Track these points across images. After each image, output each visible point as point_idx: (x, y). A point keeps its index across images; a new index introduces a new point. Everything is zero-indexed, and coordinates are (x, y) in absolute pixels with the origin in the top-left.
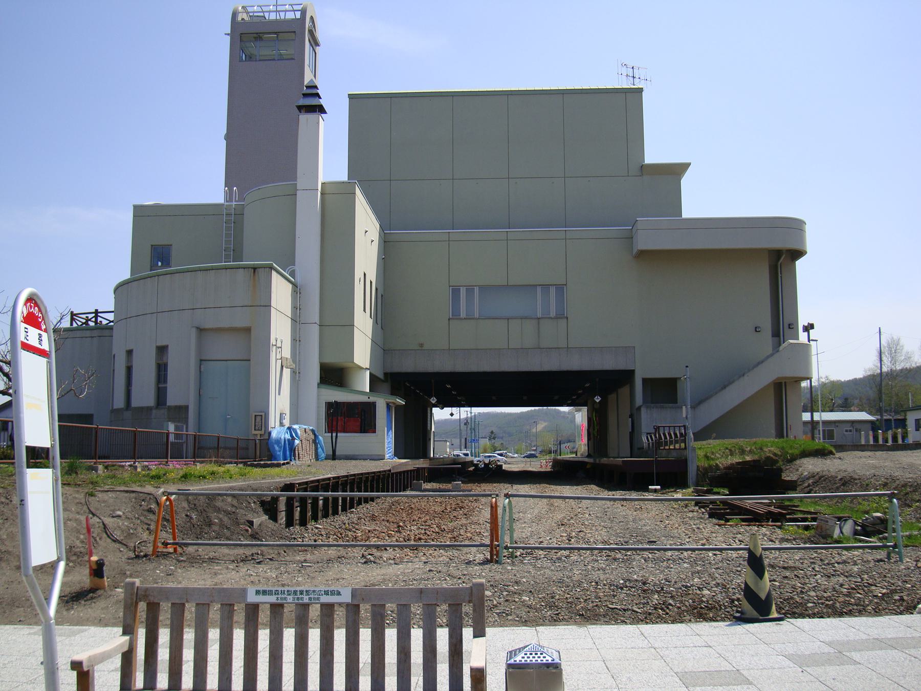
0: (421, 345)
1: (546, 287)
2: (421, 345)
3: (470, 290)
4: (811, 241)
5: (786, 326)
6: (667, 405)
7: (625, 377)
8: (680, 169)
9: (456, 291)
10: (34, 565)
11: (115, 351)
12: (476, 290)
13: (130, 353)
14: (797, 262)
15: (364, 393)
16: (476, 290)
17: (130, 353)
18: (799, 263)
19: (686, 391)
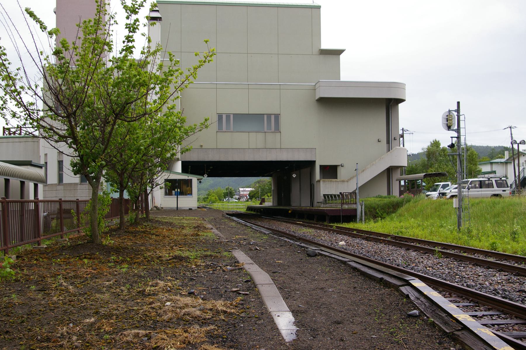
0: (201, 146)
1: (269, 116)
2: (201, 146)
3: (228, 116)
4: (408, 96)
5: (393, 138)
6: (326, 180)
7: (311, 164)
8: (338, 53)
9: (220, 117)
10: (39, 185)
11: (40, 154)
12: (232, 116)
13: (46, 155)
14: (399, 105)
15: (178, 173)
16: (232, 116)
17: (46, 155)
18: (400, 105)
19: (342, 173)
